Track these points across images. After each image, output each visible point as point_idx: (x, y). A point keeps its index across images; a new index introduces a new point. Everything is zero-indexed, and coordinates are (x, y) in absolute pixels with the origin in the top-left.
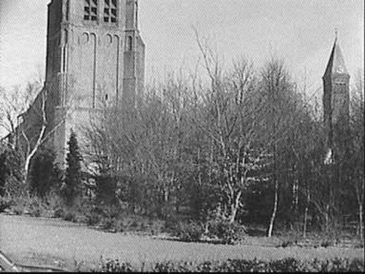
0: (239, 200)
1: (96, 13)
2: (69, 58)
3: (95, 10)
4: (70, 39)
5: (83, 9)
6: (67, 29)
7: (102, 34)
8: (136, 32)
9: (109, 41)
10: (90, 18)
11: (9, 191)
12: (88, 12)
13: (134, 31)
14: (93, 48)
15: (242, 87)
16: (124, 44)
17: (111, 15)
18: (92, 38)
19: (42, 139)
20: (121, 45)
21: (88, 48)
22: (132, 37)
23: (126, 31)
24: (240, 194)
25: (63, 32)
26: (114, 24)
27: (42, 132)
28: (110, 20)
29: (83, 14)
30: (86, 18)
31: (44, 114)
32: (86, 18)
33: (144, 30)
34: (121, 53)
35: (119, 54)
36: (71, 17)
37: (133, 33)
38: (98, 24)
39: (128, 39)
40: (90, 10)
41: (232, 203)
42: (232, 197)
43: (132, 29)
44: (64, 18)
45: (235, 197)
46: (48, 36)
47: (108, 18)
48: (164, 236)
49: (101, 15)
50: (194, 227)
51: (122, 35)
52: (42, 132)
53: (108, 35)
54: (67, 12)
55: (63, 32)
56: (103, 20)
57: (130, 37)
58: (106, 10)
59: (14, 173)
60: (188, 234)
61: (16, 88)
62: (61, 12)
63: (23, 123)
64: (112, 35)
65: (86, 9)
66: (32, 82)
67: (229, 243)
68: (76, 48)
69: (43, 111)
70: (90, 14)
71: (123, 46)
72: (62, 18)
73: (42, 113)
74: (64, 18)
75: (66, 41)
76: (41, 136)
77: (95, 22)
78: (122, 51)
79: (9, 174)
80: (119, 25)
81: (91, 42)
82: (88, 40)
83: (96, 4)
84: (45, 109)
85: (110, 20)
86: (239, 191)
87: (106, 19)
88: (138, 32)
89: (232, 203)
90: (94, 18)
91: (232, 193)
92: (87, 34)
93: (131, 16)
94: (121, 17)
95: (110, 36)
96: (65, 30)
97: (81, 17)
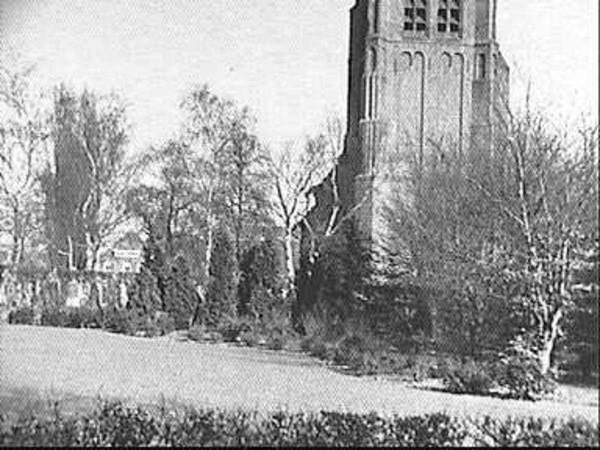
0: (559, 323)
2: (380, 96)
3: (422, 13)
4: (381, 64)
5: (403, 11)
6: (376, 47)
7: (435, 53)
8: (492, 46)
9: (447, 63)
10: (415, 26)
11: (256, 309)
12: (412, 17)
13: (489, 46)
14: (420, 79)
16: (472, 67)
17: (450, 19)
19: (333, 228)
20: (468, 70)
21: (411, 79)
22: (486, 54)
25: (370, 53)
26: (456, 35)
27: (333, 217)
28: (448, 29)
29: (401, 20)
30: (408, 26)
36: (382, 25)
37: (486, 47)
38: (428, 35)
39: (478, 58)
40: (415, 13)
42: (546, 319)
43: (485, 41)
44: (371, 29)
46: (350, 62)
47: (445, 26)
48: (435, 383)
49: (433, 20)
50: (473, 369)
51: (469, 53)
52: (333, 217)
53: (445, 53)
54: (376, 21)
55: (370, 53)
56: (436, 28)
57: (482, 56)
58: (442, 13)
59: (264, 280)
60: (458, 380)
61: (289, 145)
62: (366, 17)
64: (452, 54)
65: (408, 12)
67: (527, 397)
68: (390, 76)
69: (334, 183)
70: (415, 19)
71: (471, 72)
72: (367, 30)
73: (332, 186)
74: (371, 29)
76: (331, 223)
77: (423, 33)
78: (468, 79)
79: (257, 282)
80: (464, 35)
81: (416, 69)
84: (336, 181)
85: (448, 29)
88: (497, 45)
89: (545, 329)
90: (421, 27)
92: (409, 53)
93: (484, 22)
94: (468, 22)
95: (448, 55)
97: (399, 26)
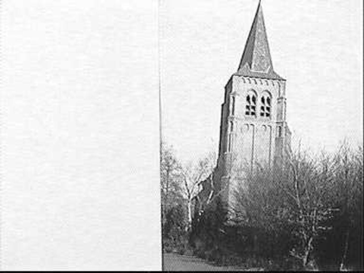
0: (311, 243)
1: (255, 110)
3: (254, 108)
10: (250, 113)
12: (249, 109)
15: (347, 172)
17: (266, 111)
18: (251, 127)
22: (281, 126)
23: (277, 123)
24: (311, 239)
25: (230, 124)
26: (268, 118)
27: (211, 195)
30: (247, 113)
31: (212, 181)
32: (247, 113)
33: (291, 122)
34: (273, 140)
35: (252, 145)
36: (235, 113)
41: (305, 247)
45: (308, 242)
49: (258, 111)
52: (211, 195)
55: (230, 124)
57: (280, 127)
58: (262, 108)
63: (202, 191)
64: (266, 126)
65: (248, 107)
66: (202, 160)
75: (232, 130)
80: (272, 118)
82: (248, 129)
83: (255, 103)
85: (265, 115)
86: (310, 237)
87: (262, 114)
90: (253, 114)
91: (306, 238)
96: (231, 122)
